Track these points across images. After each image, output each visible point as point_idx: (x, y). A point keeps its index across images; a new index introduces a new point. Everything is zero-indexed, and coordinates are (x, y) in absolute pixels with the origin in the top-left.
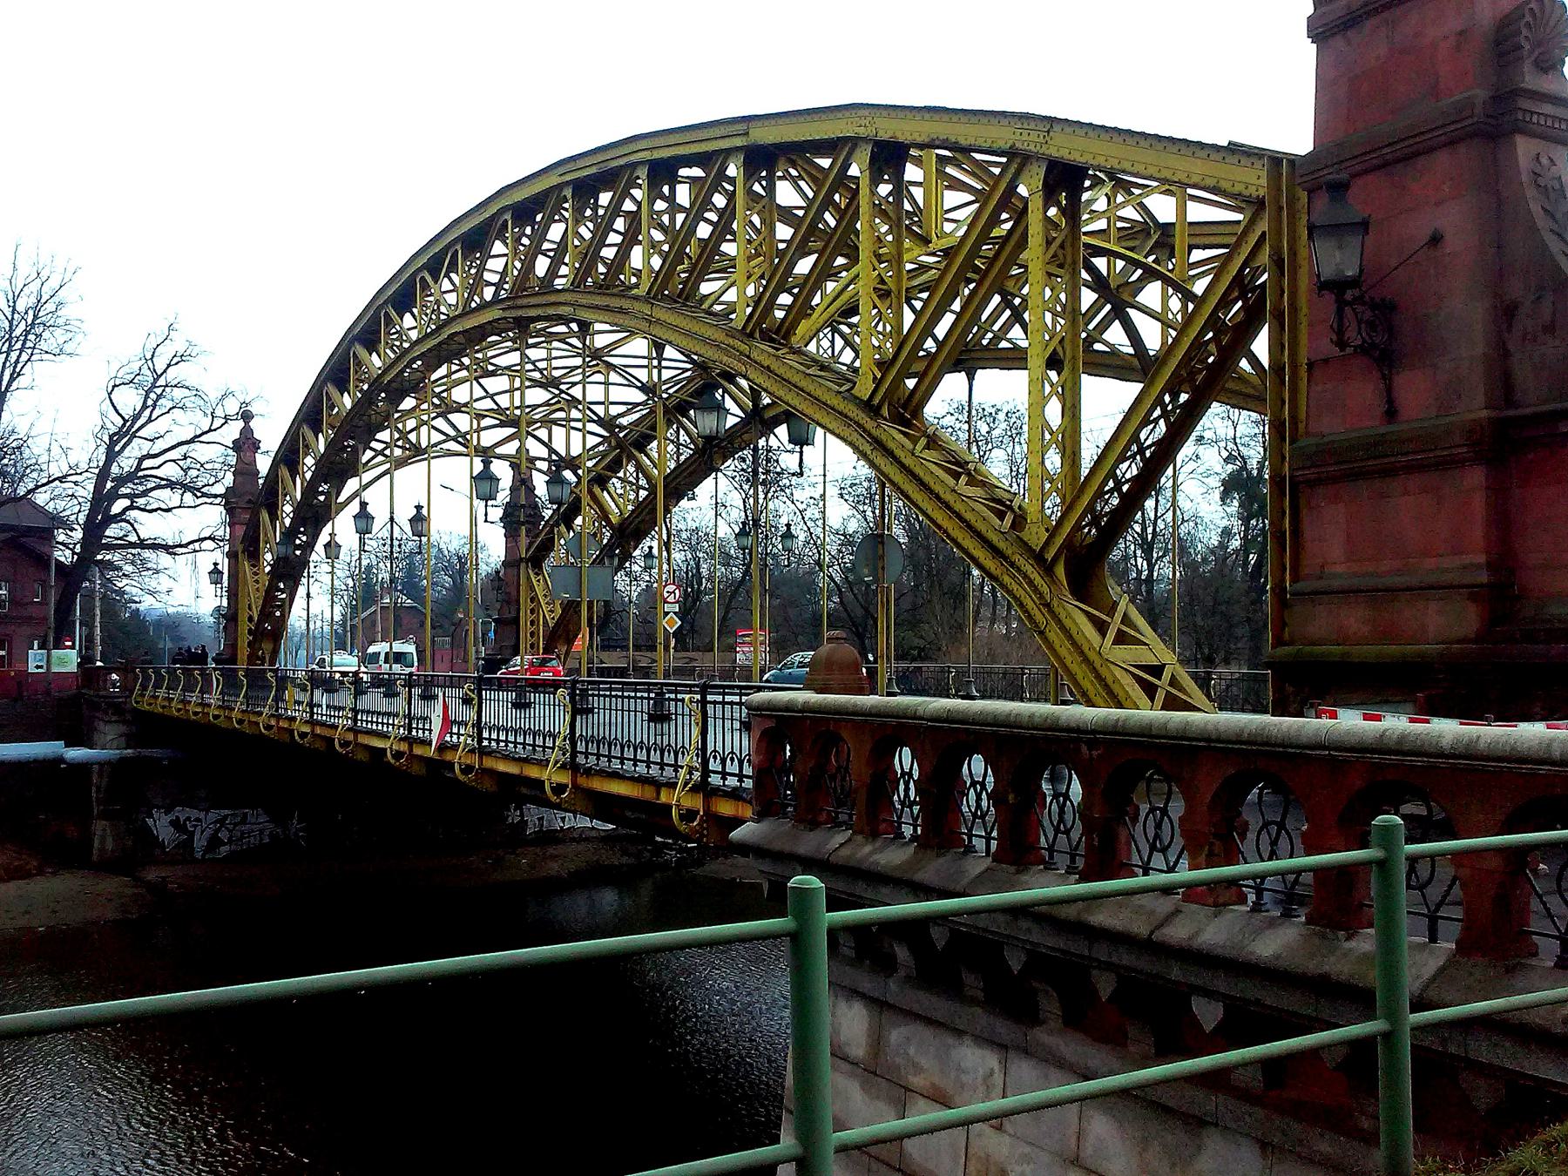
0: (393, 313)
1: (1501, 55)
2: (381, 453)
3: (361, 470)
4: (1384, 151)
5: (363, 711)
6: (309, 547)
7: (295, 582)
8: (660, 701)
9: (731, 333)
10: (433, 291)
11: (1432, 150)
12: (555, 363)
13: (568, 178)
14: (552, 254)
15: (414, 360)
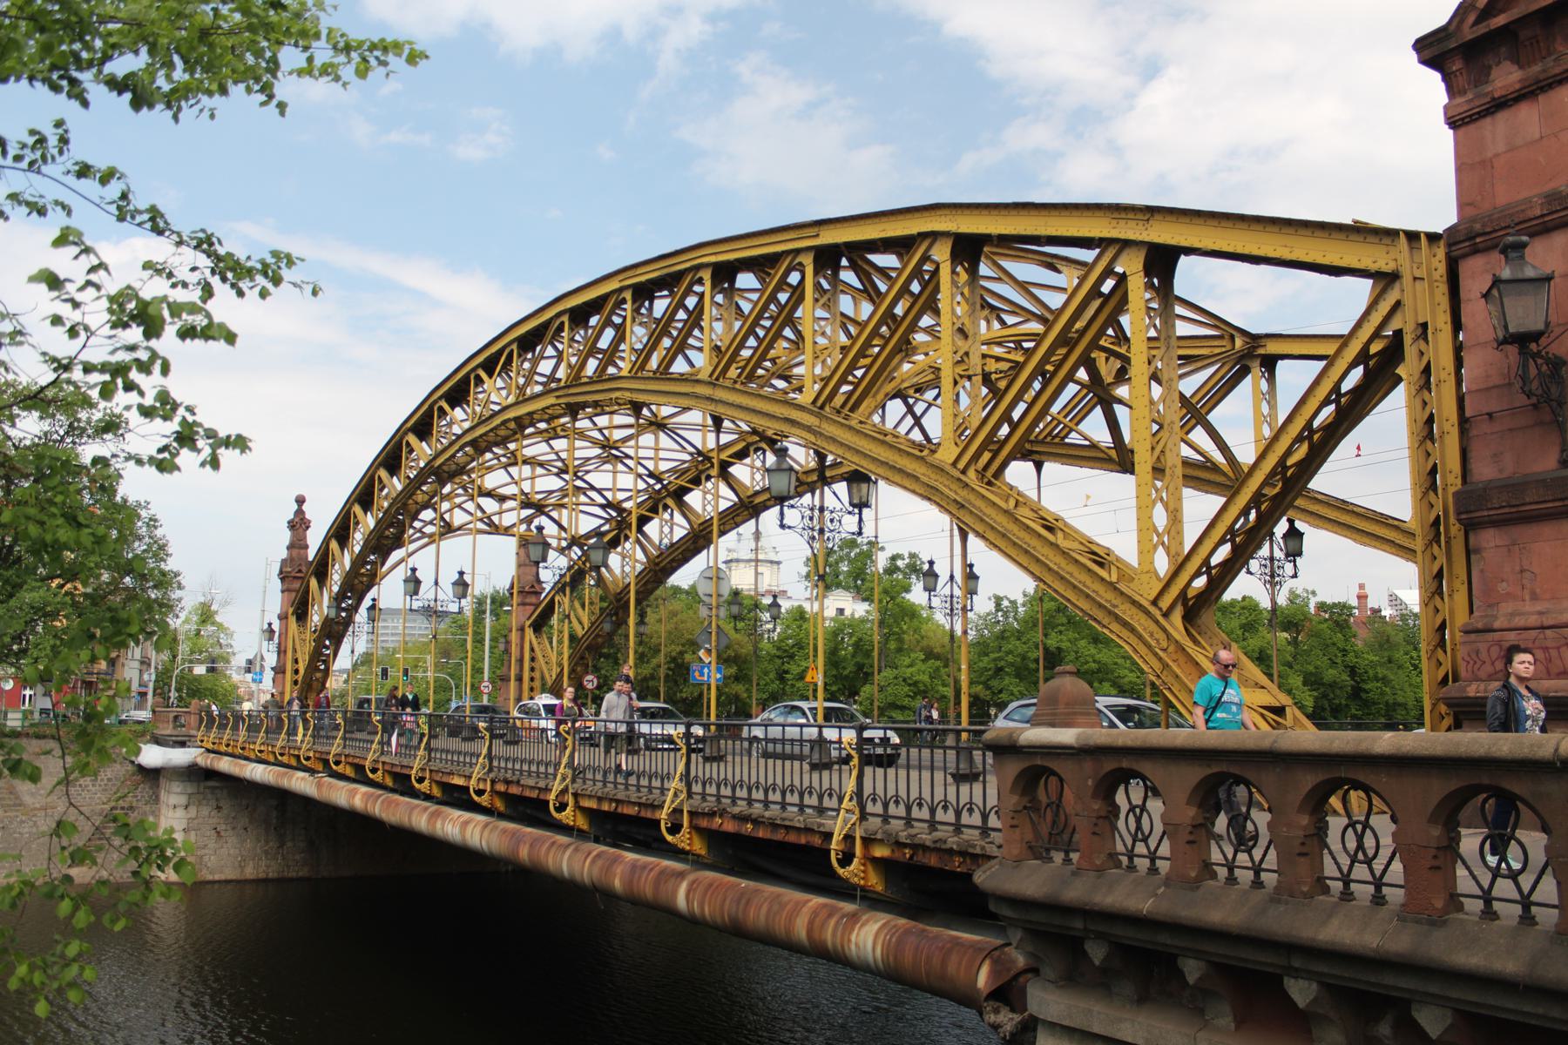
0: (446, 407)
2: (420, 530)
6: (356, 608)
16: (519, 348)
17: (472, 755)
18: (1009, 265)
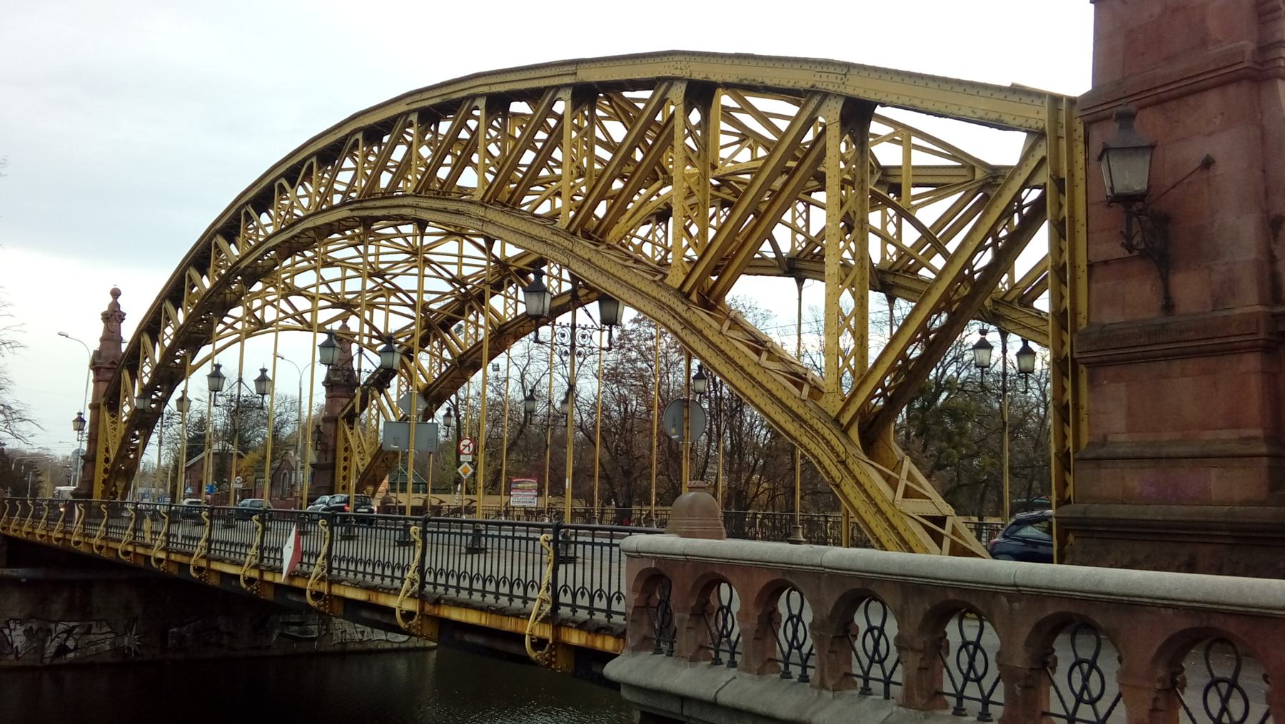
0: (253, 212)
1: (1260, 15)
2: (231, 326)
3: (215, 337)
4: (1159, 91)
5: (217, 541)
6: (164, 401)
7: (148, 430)
8: (477, 535)
9: (556, 232)
10: (288, 195)
11: (1207, 89)
12: (382, 258)
13: (414, 106)
14: (394, 170)
15: (268, 251)
16: (317, 161)
17: (194, 539)
18: (750, 99)
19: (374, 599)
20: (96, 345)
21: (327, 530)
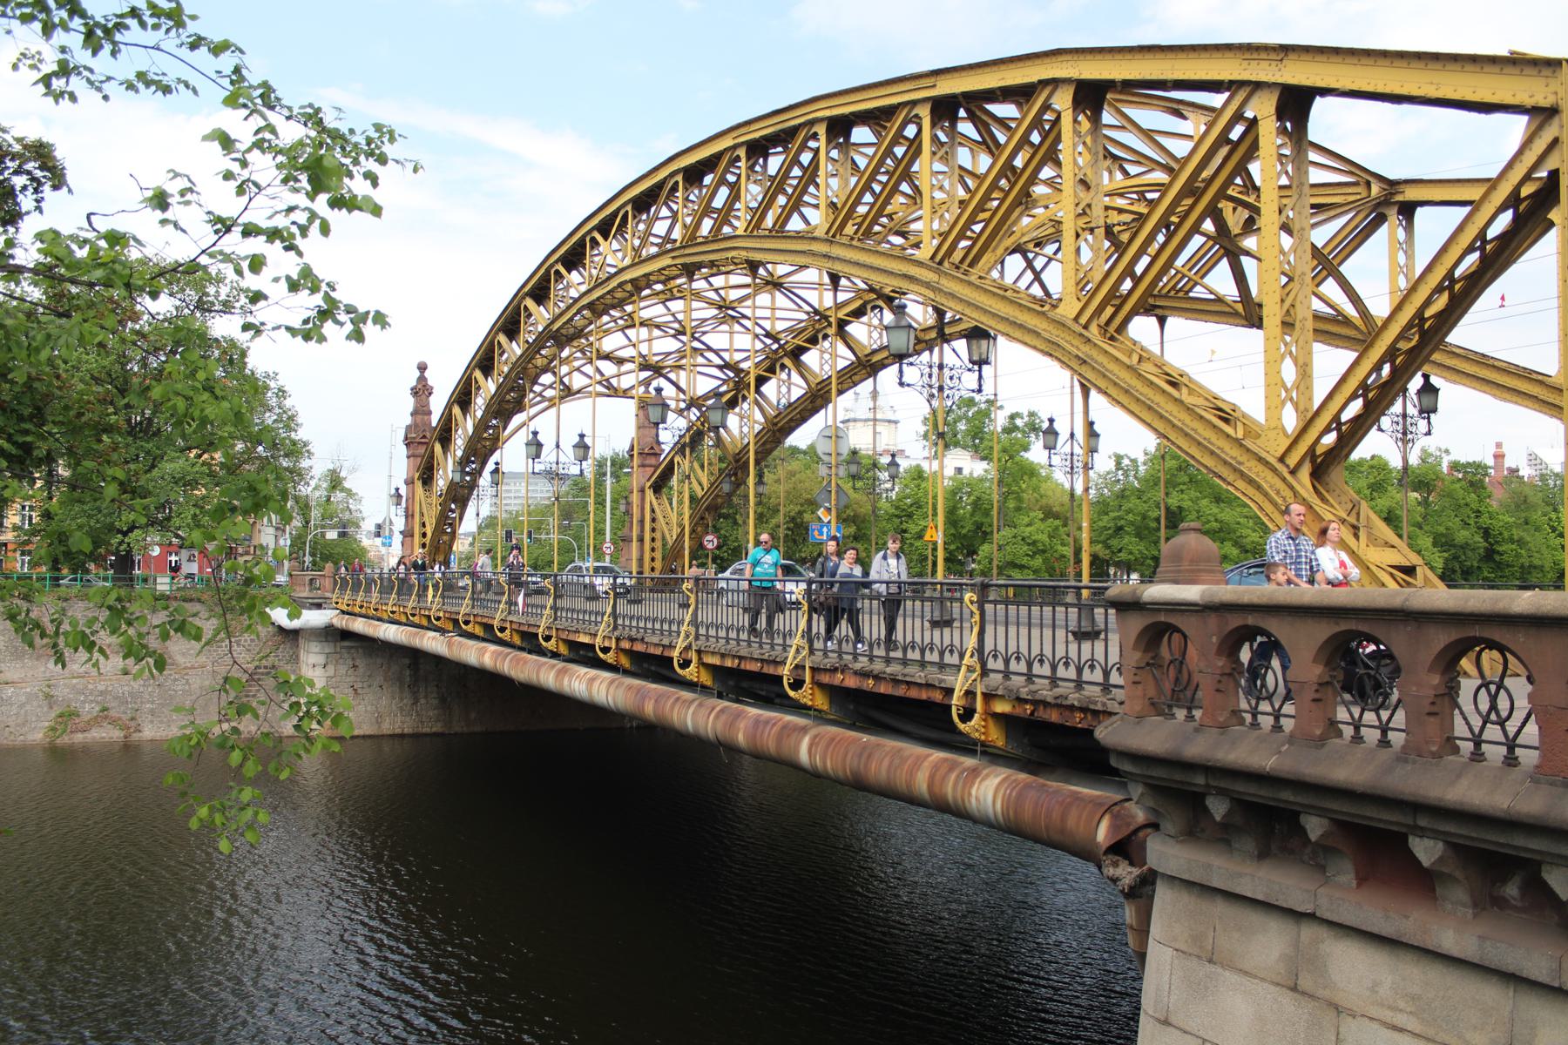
2: (540, 394)
5: (562, 609)
6: (480, 472)
19: (765, 670)
20: (408, 420)
21: (974, 608)
